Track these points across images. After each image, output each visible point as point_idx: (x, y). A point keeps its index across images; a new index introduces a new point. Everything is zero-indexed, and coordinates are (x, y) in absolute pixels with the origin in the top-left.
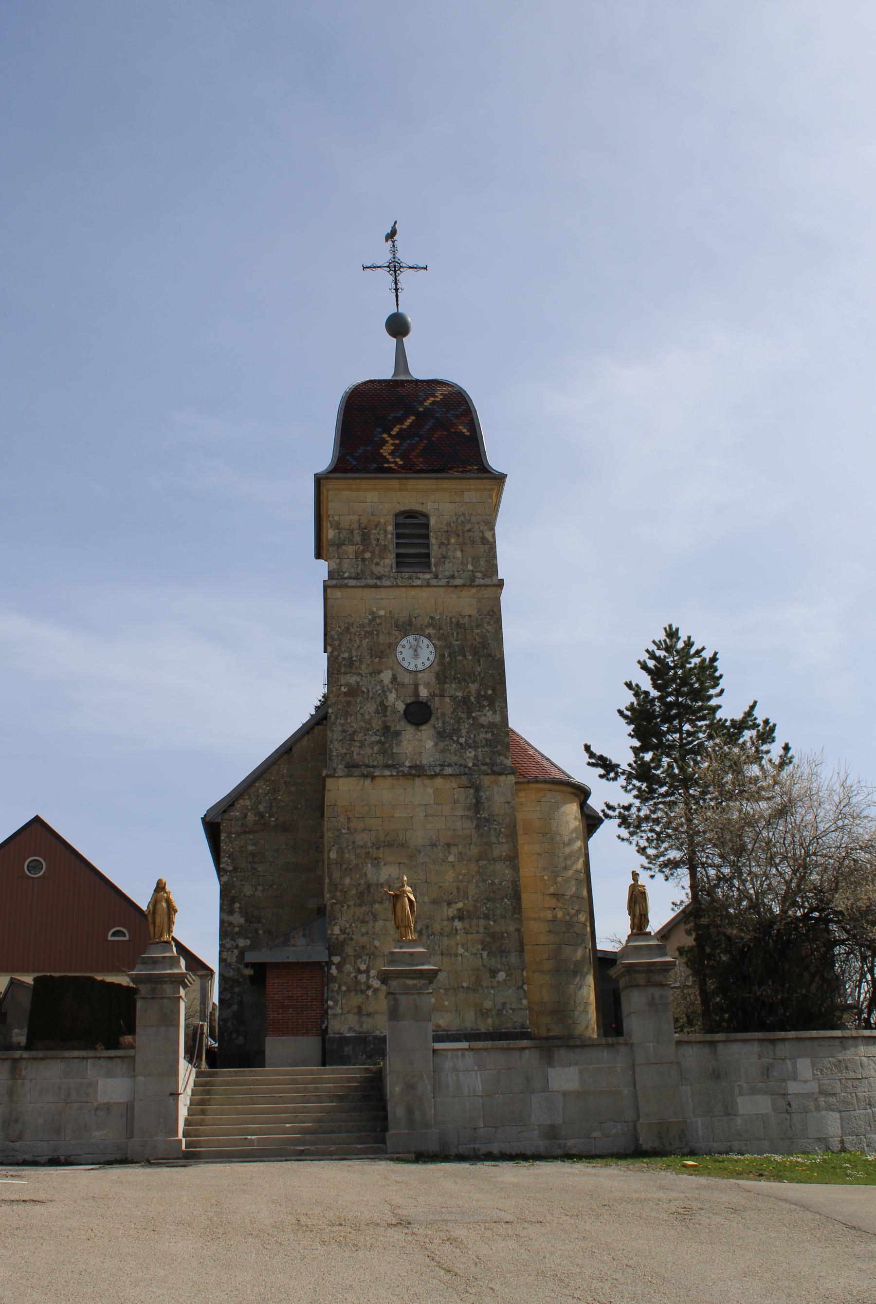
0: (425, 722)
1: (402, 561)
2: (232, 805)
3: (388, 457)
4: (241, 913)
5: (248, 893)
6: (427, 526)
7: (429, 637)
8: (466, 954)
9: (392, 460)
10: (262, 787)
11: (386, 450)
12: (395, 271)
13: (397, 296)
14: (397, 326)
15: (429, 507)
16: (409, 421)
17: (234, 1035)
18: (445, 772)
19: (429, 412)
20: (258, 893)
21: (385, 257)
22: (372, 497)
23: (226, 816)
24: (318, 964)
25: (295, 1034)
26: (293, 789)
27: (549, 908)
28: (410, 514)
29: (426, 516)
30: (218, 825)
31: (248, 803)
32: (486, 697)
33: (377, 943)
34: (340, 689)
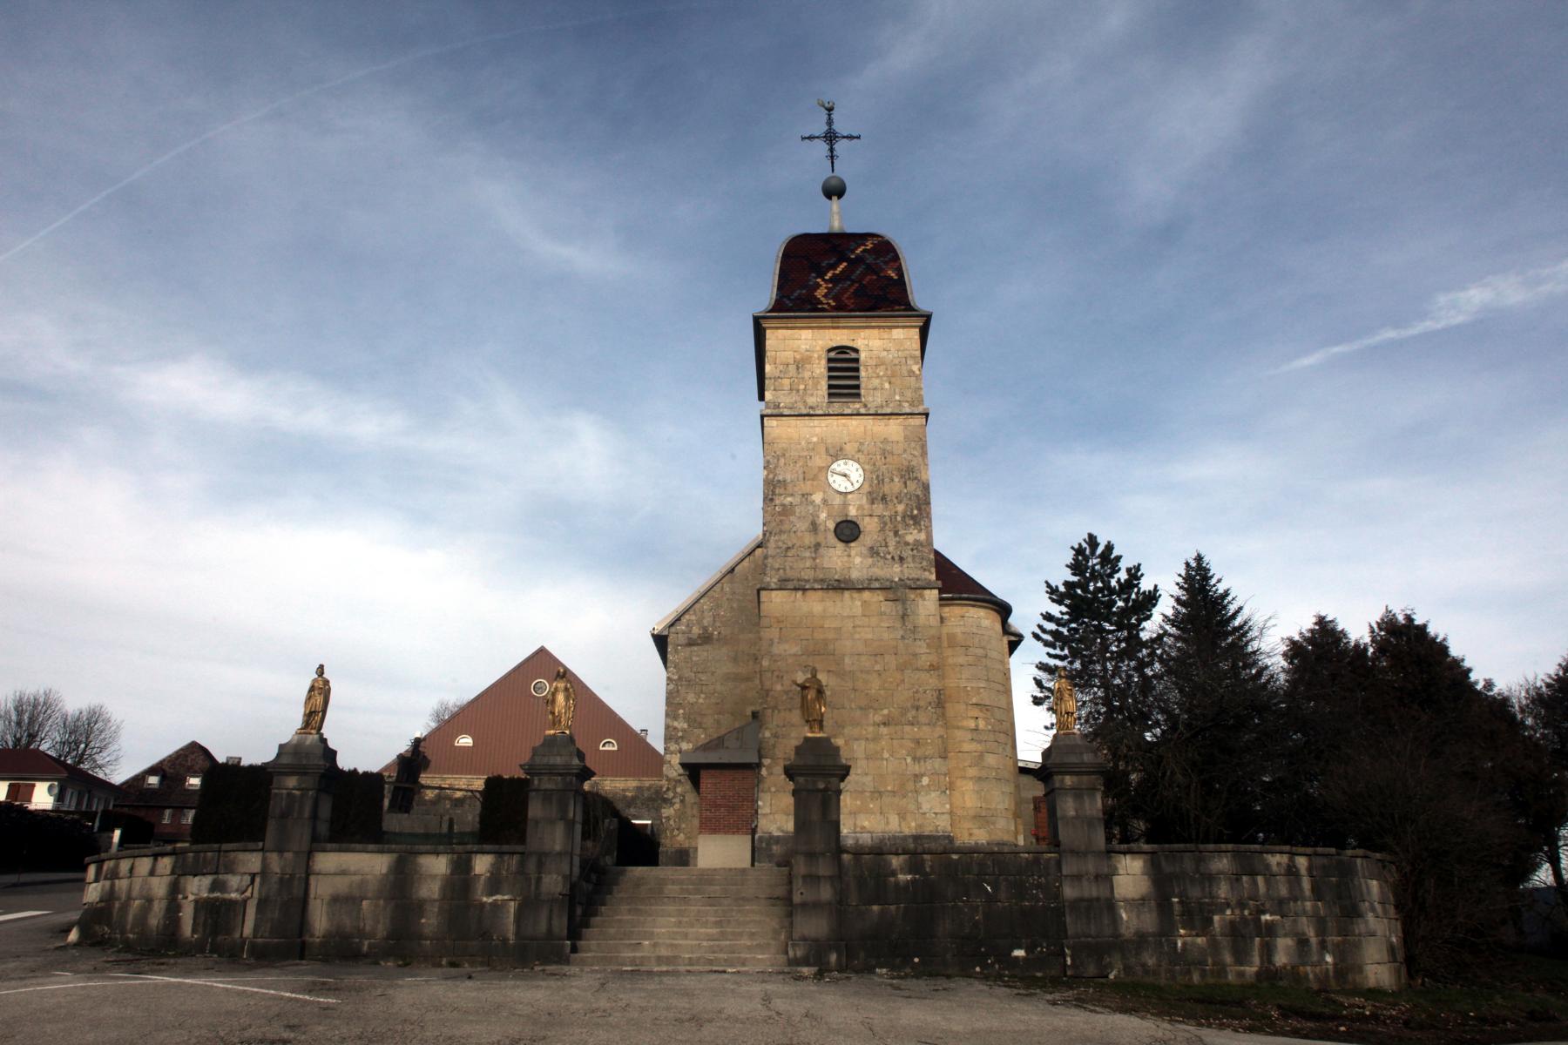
0: (855, 539)
1: (835, 392)
2: (678, 619)
6: (857, 360)
7: (858, 461)
10: (706, 604)
11: (820, 293)
15: (859, 344)
19: (860, 260)
21: (821, 128)
22: (806, 334)
28: (842, 349)
29: (856, 351)
30: (666, 637)
32: (913, 517)
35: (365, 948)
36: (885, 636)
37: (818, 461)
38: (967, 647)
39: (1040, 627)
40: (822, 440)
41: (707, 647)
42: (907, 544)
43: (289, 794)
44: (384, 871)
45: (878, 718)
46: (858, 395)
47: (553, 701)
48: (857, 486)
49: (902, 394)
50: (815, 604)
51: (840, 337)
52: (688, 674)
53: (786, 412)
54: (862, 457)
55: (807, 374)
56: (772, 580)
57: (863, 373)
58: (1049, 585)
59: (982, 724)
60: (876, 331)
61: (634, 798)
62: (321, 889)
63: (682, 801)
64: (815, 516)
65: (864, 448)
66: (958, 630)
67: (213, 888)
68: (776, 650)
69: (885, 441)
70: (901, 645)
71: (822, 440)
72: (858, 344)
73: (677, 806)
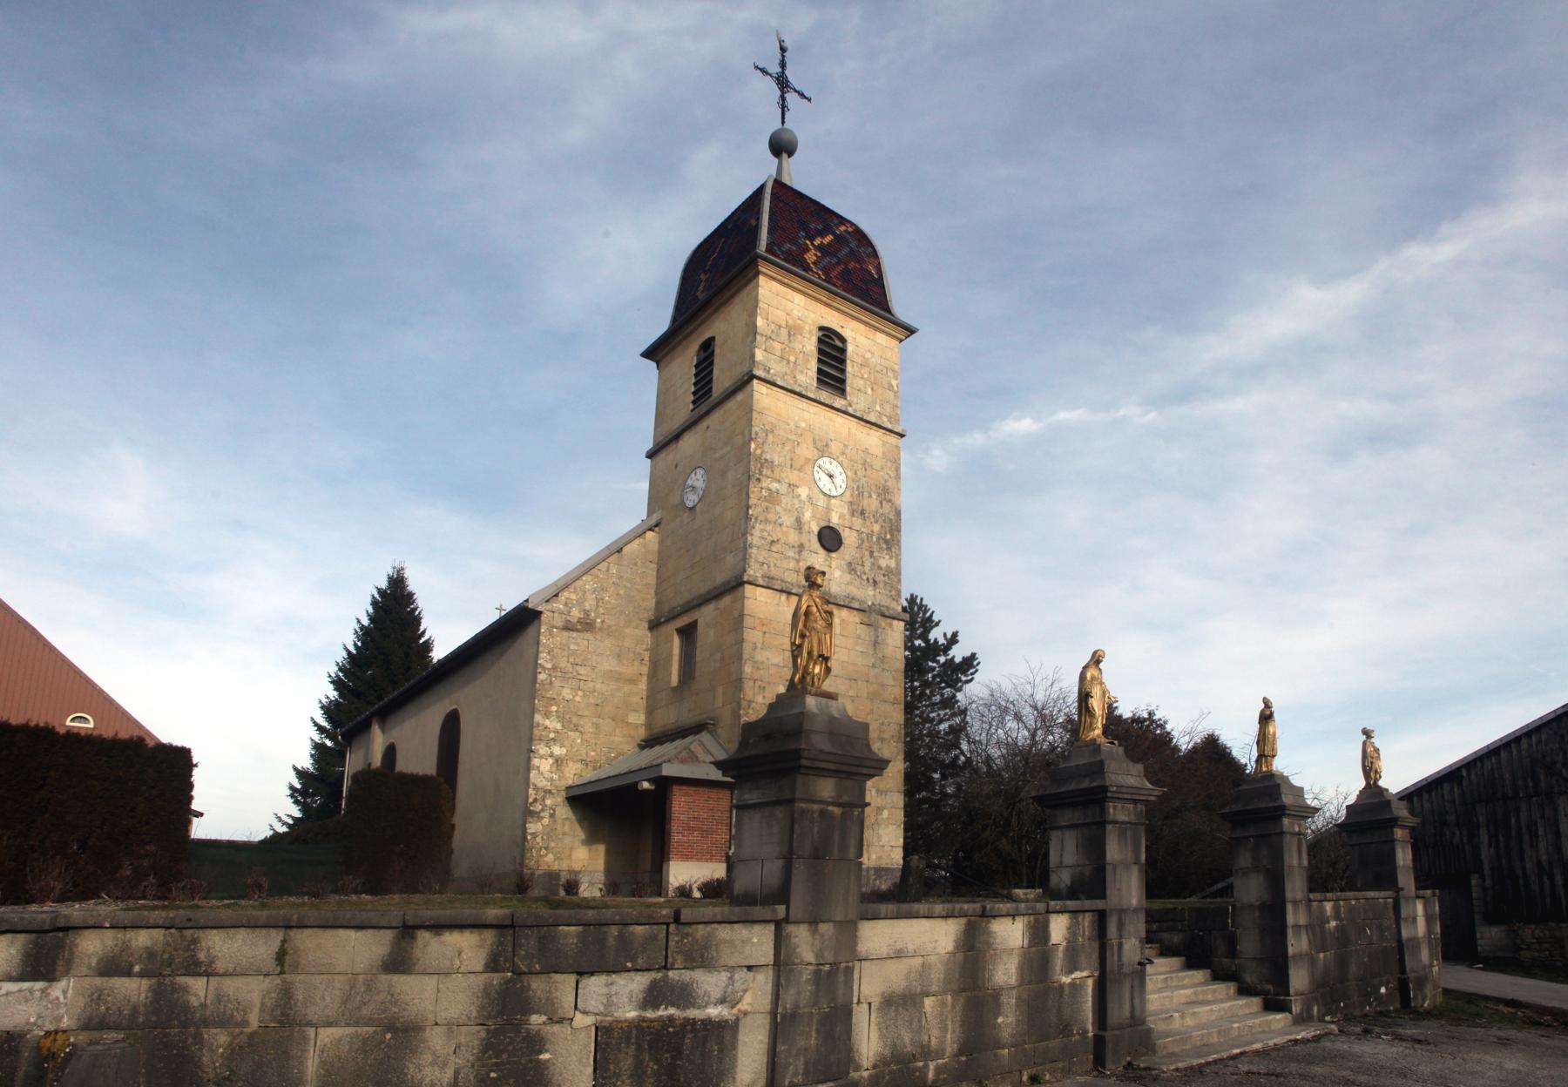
5: (569, 697)
14: (781, 147)
17: (543, 852)
20: (578, 699)
22: (799, 299)
25: (699, 860)
29: (843, 340)
31: (573, 597)
32: (886, 542)
35: (931, 1075)
41: (588, 635)
42: (880, 568)
43: (823, 813)
44: (950, 947)
49: (882, 406)
51: (833, 320)
52: (563, 664)
55: (798, 347)
62: (871, 984)
63: (552, 816)
67: (653, 997)
69: (866, 451)
72: (846, 333)
73: (546, 821)
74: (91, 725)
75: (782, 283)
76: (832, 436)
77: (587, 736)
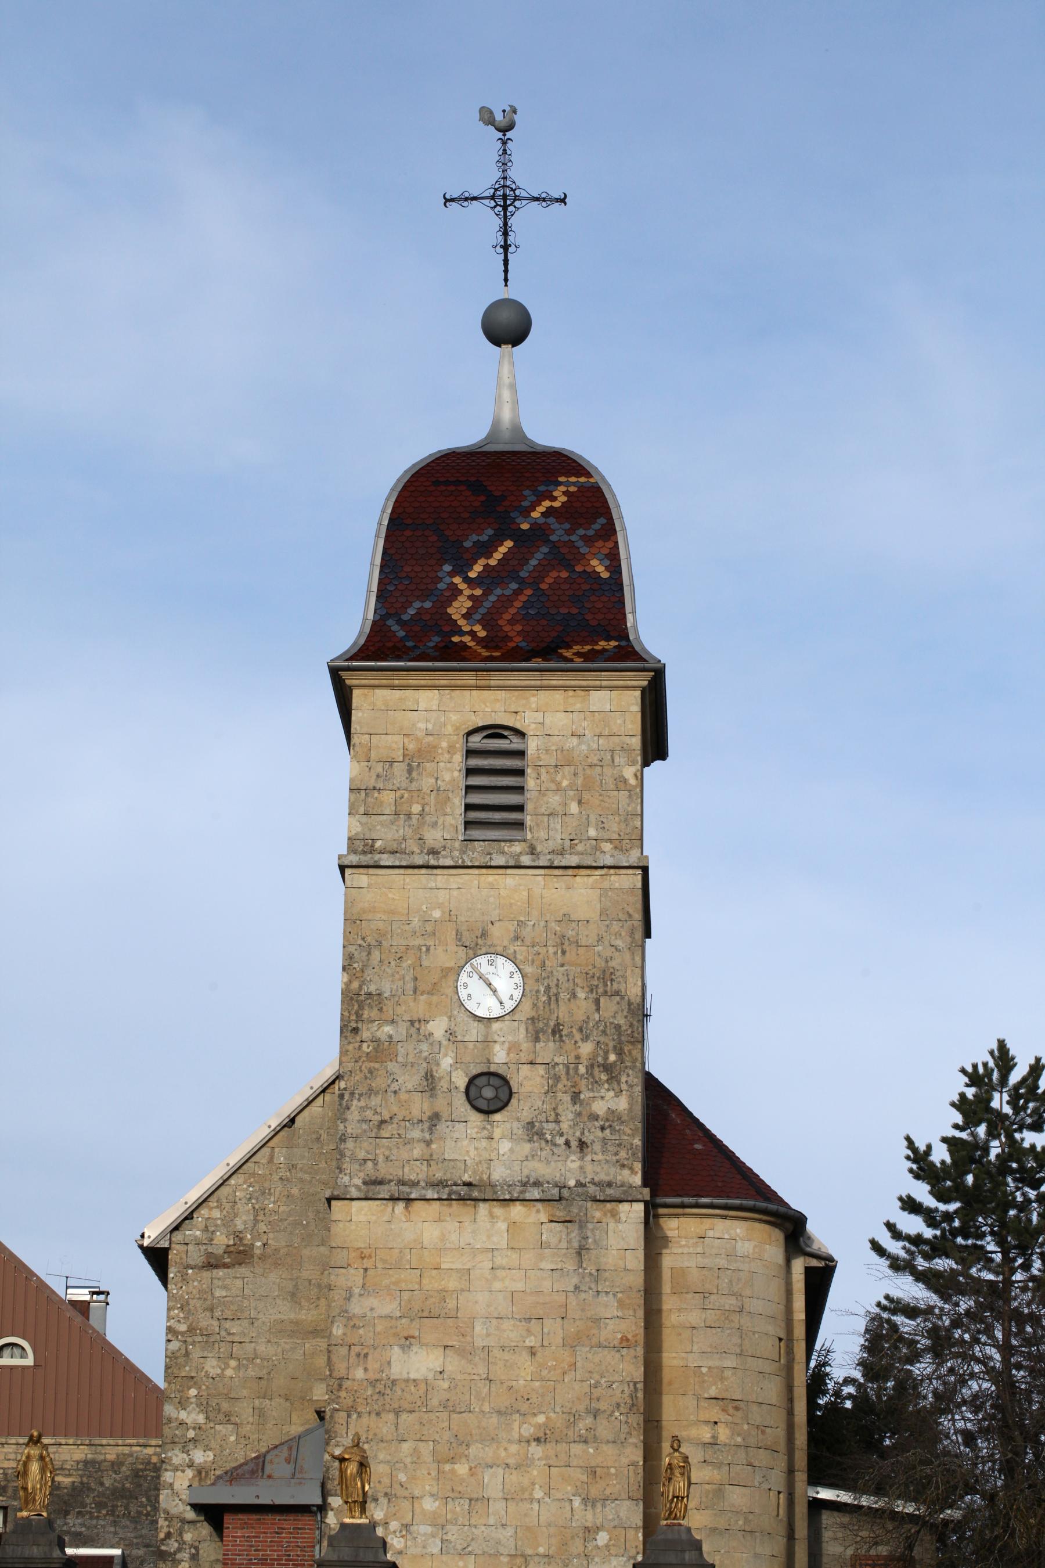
3: (461, 622)
4: (199, 1405)
5: (213, 1372)
6: (521, 754)
8: (547, 1499)
9: (467, 629)
12: (505, 208)
13: (506, 262)
16: (503, 549)
18: (528, 1196)
19: (539, 532)
20: (229, 1372)
21: (485, 180)
22: (427, 699)
23: (178, 1236)
24: (303, 1509)
26: (295, 1191)
27: (707, 1422)
28: (495, 731)
29: (521, 734)
30: (165, 1251)
31: (216, 1214)
32: (607, 1068)
33: (402, 1477)
34: (360, 1047)
36: (546, 1285)
37: (443, 957)
38: (705, 1294)
39: (890, 1227)
40: (450, 916)
41: (242, 1270)
42: (595, 1117)
45: (528, 1431)
46: (520, 825)
47: (24, 1473)
48: (509, 1005)
49: (602, 826)
50: (428, 1227)
52: (205, 1321)
53: (386, 860)
54: (522, 952)
56: (353, 1180)
57: (530, 782)
58: (910, 1143)
59: (723, 1434)
60: (558, 695)
61: (78, 1491)
63: (194, 1557)
64: (432, 1061)
65: (527, 932)
66: (691, 1263)
68: (356, 1308)
70: (573, 1301)
71: (450, 916)
74: (29, 1361)
75: (393, 687)
76: (494, 915)
77: (246, 1429)
